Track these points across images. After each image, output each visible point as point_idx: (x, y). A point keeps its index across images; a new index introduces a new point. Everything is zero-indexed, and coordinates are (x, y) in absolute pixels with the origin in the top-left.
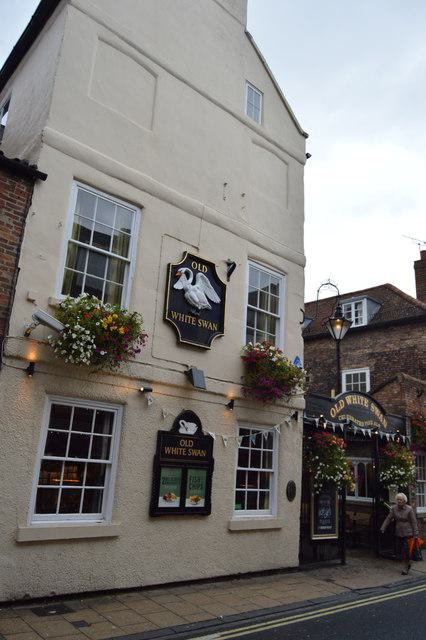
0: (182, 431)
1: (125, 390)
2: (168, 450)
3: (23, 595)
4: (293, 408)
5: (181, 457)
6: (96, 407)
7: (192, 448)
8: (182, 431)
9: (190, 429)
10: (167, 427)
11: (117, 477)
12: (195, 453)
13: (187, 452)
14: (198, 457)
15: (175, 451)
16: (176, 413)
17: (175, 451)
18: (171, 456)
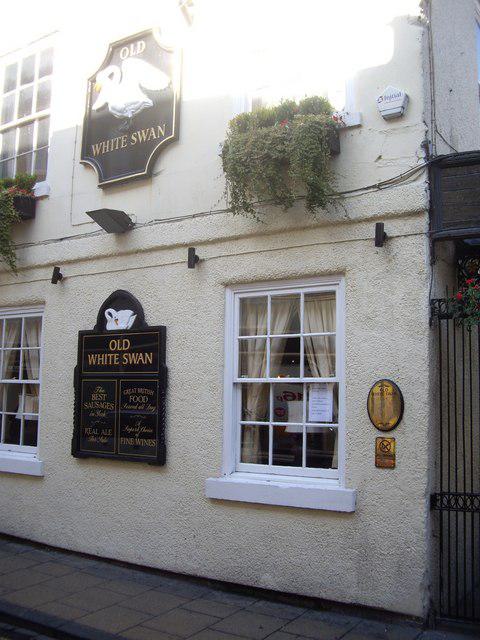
0: (111, 326)
1: (39, 286)
2: (92, 359)
3: (342, 186)
4: (368, 220)
5: (108, 367)
6: (23, 314)
7: (129, 351)
8: (111, 326)
9: (121, 320)
10: (90, 324)
11: (224, 315)
12: (134, 359)
13: (121, 359)
14: (140, 366)
15: (103, 359)
16: (394, 434)
17: (103, 359)
18: (96, 368)
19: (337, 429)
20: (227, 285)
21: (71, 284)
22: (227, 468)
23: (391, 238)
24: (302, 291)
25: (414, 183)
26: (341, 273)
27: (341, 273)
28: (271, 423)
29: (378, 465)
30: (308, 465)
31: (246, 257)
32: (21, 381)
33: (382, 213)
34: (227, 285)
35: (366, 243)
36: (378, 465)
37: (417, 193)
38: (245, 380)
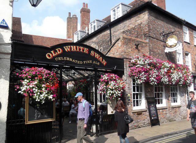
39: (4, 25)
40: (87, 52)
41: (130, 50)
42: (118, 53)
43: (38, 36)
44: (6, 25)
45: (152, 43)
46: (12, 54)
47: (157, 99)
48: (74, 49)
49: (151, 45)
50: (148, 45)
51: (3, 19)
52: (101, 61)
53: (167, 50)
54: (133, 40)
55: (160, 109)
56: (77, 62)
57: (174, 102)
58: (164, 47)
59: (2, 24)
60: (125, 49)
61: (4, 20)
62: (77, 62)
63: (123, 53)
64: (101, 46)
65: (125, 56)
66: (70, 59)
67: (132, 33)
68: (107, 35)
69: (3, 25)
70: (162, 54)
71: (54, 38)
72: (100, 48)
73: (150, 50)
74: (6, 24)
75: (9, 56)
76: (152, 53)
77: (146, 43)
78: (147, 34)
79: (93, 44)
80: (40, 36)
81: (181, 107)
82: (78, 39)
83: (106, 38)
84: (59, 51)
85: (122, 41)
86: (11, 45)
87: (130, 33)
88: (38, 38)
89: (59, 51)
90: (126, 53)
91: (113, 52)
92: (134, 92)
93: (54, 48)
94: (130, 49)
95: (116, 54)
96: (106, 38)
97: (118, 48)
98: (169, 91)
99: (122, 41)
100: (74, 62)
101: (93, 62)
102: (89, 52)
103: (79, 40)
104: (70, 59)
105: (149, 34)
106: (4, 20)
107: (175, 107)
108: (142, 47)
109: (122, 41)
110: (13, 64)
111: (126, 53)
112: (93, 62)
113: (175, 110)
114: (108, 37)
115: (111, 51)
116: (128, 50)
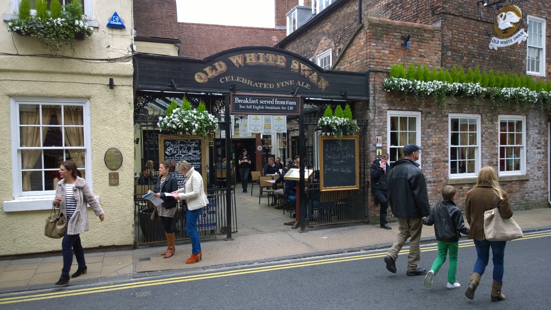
19: (84, 170)
20: (11, 96)
21: (117, 89)
22: (15, 194)
23: (115, 86)
24: (41, 104)
25: (127, 63)
26: (88, 98)
27: (88, 98)
28: (505, 159)
29: (111, 184)
30: (46, 190)
31: (26, 82)
32: (63, 147)
33: (112, 73)
34: (11, 96)
35: (102, 86)
36: (111, 184)
37: (128, 67)
38: (24, 148)
39: (117, 23)
40: (283, 64)
41: (387, 52)
42: (358, 61)
43: (213, 25)
44: (120, 23)
45: (452, 30)
46: (134, 76)
47: (505, 159)
48: (251, 60)
49: (449, 34)
50: (438, 35)
51: (114, 12)
52: (300, 85)
53: (496, 44)
54: (396, 28)
55: (464, 184)
56: (262, 86)
57: (508, 170)
58: (489, 35)
59: (114, 23)
60: (374, 51)
61: (116, 14)
62: (262, 86)
63: (368, 60)
64: (339, 42)
65: (372, 66)
66: (247, 82)
67: (407, 8)
68: (350, 14)
69: (115, 23)
70: (480, 55)
71: (247, 28)
72: (338, 48)
73: (443, 47)
74: (120, 21)
75: (130, 82)
76: (449, 54)
77: (432, 31)
78: (438, 7)
79: (324, 38)
80: (217, 26)
81: (528, 180)
82: (294, 28)
83: (351, 21)
84: (221, 66)
85: (368, 31)
86: (132, 60)
87: (400, 7)
88: (212, 30)
89: (221, 66)
90: (376, 60)
91: (350, 59)
92: (393, 147)
93: (210, 61)
94: (387, 49)
95: (355, 62)
96: (351, 21)
97: (358, 48)
98: (494, 144)
99: (368, 31)
100: (257, 86)
101: (296, 82)
102: (289, 63)
103: (296, 29)
104: (247, 82)
105: (444, 8)
106: (116, 14)
107: (511, 181)
108: (422, 41)
109: (367, 33)
110: (138, 94)
111: (376, 60)
112: (296, 82)
113: (511, 187)
114: (356, 20)
115: (347, 59)
116: (383, 51)
